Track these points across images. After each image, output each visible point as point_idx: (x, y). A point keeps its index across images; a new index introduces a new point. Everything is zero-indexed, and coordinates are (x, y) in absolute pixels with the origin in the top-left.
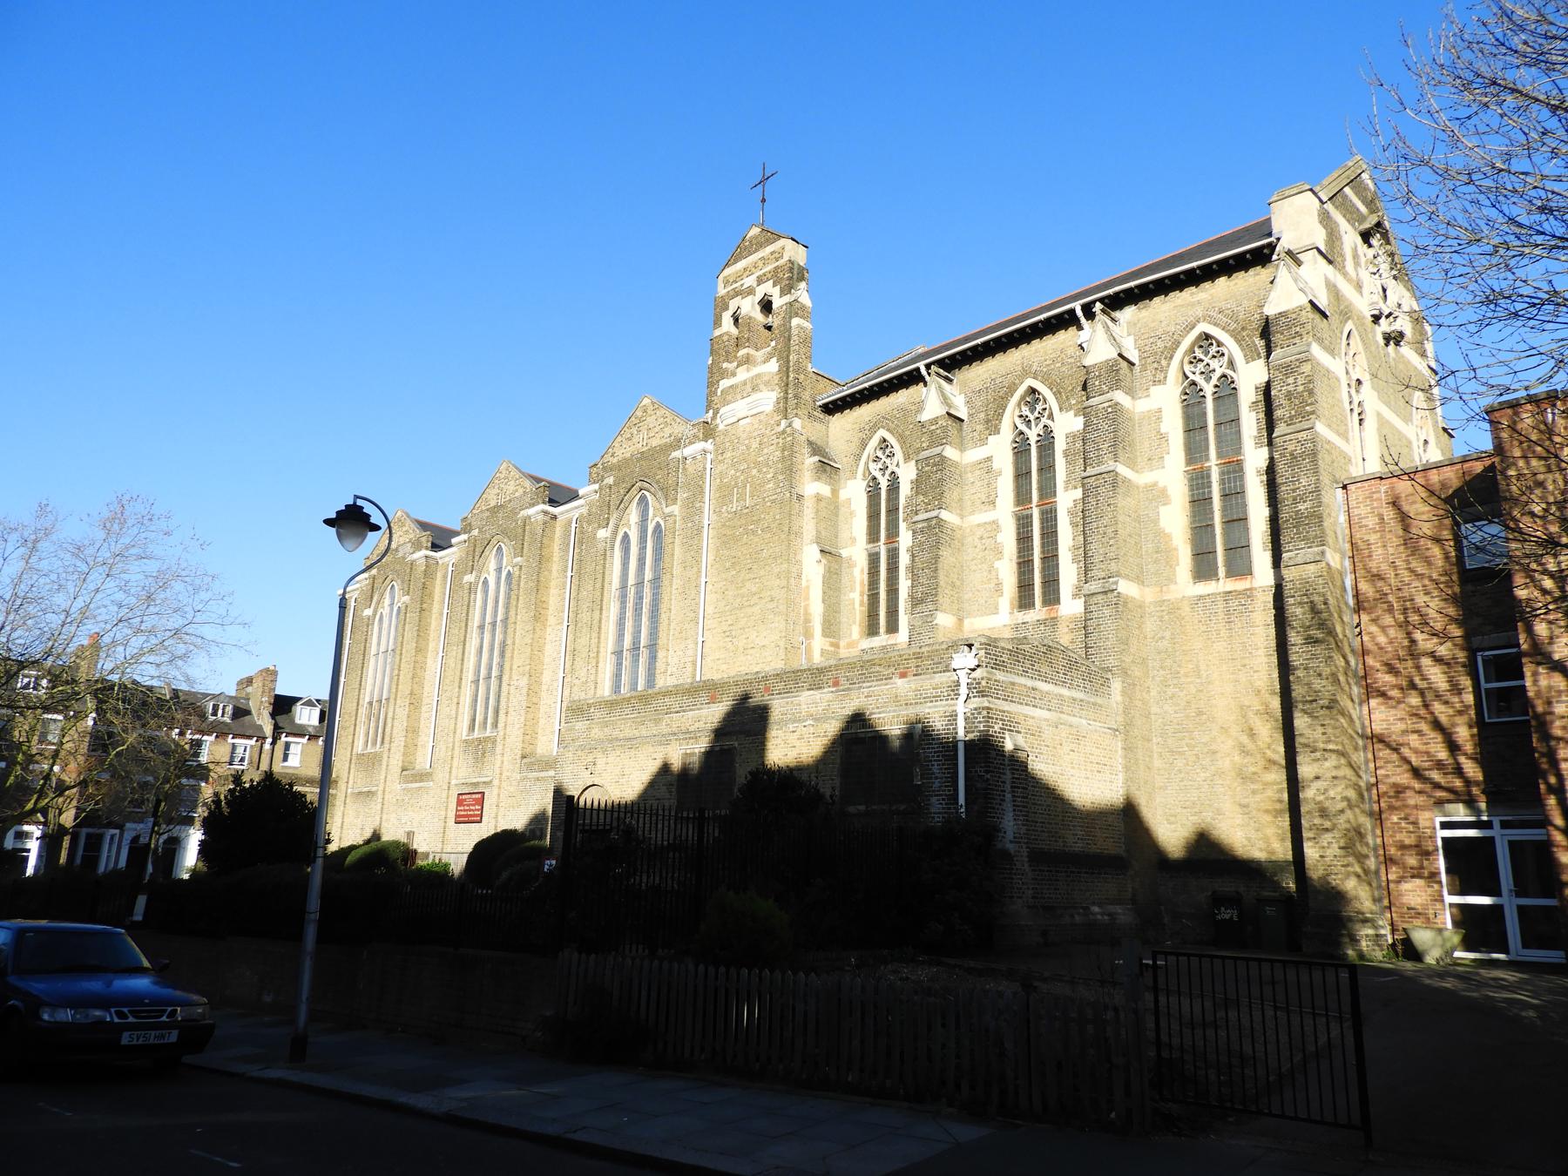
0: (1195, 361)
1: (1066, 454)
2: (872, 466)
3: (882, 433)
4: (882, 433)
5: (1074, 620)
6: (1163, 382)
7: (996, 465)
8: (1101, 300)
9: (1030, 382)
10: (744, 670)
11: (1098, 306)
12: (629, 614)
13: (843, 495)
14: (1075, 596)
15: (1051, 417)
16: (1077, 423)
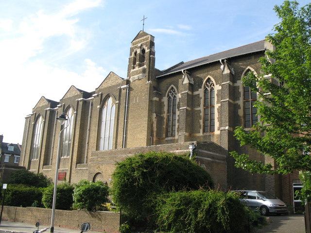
0: (171, 92)
1: (217, 95)
2: (169, 94)
3: (172, 86)
4: (172, 86)
5: (218, 135)
6: (201, 88)
7: (200, 96)
8: (226, 59)
9: (209, 76)
10: (175, 77)
11: (225, 61)
12: (121, 119)
13: (163, 100)
14: (218, 130)
15: (214, 85)
16: (220, 88)
